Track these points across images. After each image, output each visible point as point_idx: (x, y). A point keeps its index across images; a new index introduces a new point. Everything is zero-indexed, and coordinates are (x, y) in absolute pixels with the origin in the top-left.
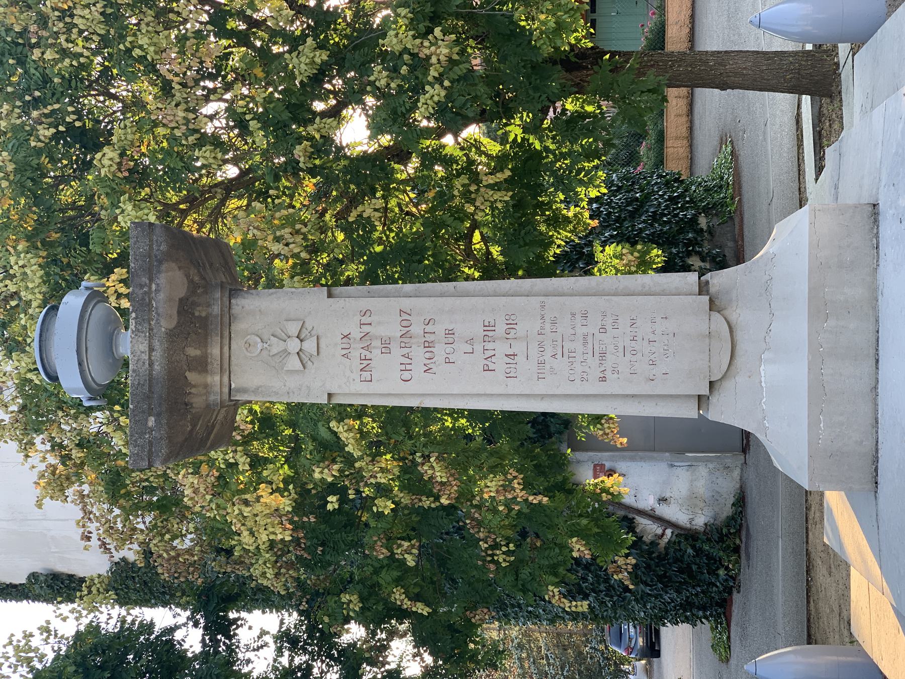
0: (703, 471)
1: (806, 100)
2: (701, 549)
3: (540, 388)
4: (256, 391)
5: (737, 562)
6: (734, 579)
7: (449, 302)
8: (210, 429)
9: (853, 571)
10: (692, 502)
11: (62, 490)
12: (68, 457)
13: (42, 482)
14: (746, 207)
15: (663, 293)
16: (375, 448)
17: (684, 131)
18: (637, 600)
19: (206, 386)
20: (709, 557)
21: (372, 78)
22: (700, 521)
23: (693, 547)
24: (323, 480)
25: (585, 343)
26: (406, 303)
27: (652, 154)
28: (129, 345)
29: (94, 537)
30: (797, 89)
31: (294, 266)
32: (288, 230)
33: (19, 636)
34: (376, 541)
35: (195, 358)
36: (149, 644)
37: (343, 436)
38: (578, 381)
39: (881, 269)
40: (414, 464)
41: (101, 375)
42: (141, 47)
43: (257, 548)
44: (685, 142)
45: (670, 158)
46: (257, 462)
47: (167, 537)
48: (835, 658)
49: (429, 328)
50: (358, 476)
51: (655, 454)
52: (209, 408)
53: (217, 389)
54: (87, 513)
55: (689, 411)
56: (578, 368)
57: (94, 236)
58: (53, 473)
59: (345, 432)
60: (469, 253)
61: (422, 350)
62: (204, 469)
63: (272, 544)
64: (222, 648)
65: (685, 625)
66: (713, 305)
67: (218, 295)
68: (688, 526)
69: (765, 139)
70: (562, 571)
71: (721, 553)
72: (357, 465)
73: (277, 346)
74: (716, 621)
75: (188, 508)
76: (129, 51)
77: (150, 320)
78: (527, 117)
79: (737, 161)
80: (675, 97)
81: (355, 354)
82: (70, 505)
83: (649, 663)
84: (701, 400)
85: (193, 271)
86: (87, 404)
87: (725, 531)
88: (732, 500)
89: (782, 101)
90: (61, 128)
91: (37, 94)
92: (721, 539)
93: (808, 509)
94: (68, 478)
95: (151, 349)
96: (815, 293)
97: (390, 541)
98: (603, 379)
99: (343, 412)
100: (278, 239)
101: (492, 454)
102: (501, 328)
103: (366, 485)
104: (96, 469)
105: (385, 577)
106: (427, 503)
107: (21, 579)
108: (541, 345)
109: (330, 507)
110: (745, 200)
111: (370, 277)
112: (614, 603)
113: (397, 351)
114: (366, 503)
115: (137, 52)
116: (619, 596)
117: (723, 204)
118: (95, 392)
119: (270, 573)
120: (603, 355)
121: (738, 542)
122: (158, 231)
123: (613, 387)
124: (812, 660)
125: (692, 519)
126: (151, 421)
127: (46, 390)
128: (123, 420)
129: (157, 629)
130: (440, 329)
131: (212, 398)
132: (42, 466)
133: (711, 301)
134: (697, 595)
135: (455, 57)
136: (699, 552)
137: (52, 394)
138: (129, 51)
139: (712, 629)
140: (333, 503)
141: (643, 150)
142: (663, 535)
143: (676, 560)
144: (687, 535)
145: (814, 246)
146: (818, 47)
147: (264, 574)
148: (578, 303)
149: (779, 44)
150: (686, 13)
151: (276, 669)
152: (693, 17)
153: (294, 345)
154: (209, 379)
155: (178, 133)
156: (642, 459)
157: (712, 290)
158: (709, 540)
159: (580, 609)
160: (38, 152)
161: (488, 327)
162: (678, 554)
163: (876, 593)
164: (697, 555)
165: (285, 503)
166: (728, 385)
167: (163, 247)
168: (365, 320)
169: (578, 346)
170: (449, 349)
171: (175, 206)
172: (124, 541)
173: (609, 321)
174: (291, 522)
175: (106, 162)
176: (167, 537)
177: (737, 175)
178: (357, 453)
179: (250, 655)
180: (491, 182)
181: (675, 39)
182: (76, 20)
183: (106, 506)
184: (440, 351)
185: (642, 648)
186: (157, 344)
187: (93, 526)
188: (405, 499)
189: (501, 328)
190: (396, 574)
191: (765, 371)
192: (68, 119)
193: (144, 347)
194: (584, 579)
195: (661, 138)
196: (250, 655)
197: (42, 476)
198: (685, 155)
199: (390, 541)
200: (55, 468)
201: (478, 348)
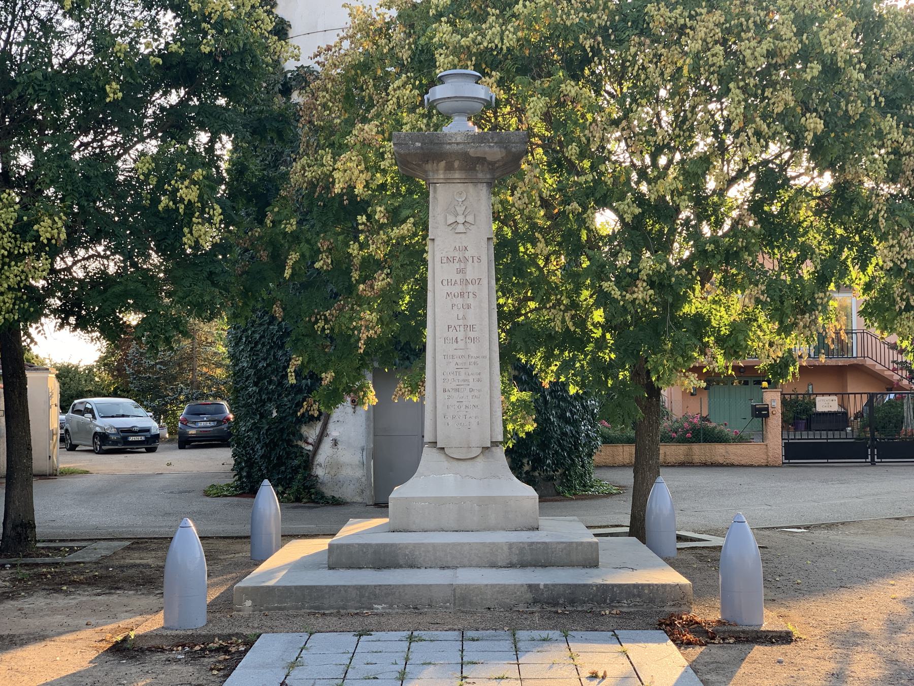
0: (359, 473)
2: (298, 472)
3: (439, 357)
4: (435, 198)
7: (486, 305)
10: (336, 465)
14: (567, 503)
15: (492, 423)
18: (254, 424)
19: (437, 170)
20: (292, 479)
21: (623, 250)
22: (319, 472)
23: (299, 466)
25: (464, 381)
26: (485, 282)
34: (329, 240)
38: (443, 377)
40: (382, 269)
44: (628, 461)
45: (614, 449)
51: (372, 436)
55: (428, 438)
56: (451, 377)
58: (371, 24)
61: (459, 291)
65: (233, 462)
67: (488, 176)
68: (316, 463)
69: (615, 513)
70: (312, 366)
71: (295, 488)
73: (460, 210)
74: (236, 487)
79: (604, 497)
81: (456, 254)
85: (501, 163)
87: (313, 491)
88: (337, 496)
92: (305, 488)
95: (458, 144)
96: (492, 499)
97: (329, 250)
98: (445, 391)
102: (472, 334)
103: (367, 237)
105: (305, 247)
106: (355, 275)
110: (572, 502)
112: (251, 405)
116: (257, 409)
117: (570, 488)
120: (457, 390)
121: (304, 500)
123: (440, 395)
124: (273, 520)
125: (321, 466)
126: (418, 144)
130: (471, 301)
131: (431, 174)
133: (488, 448)
134: (260, 470)
135: (637, 302)
136: (295, 470)
139: (228, 485)
142: (308, 443)
143: (288, 454)
144: (308, 461)
148: (486, 376)
152: (732, 465)
153: (461, 219)
154: (441, 172)
156: (368, 426)
157: (494, 449)
158: (305, 478)
159: (290, 378)
160: (576, 39)
161: (472, 328)
162: (293, 456)
164: (293, 470)
166: (442, 457)
167: (514, 150)
169: (463, 377)
173: (476, 393)
180: (567, 318)
184: (459, 301)
185: (186, 433)
186: (461, 146)
189: (472, 334)
193: (459, 140)
194: (270, 382)
198: (617, 461)
199: (329, 250)
201: (461, 322)
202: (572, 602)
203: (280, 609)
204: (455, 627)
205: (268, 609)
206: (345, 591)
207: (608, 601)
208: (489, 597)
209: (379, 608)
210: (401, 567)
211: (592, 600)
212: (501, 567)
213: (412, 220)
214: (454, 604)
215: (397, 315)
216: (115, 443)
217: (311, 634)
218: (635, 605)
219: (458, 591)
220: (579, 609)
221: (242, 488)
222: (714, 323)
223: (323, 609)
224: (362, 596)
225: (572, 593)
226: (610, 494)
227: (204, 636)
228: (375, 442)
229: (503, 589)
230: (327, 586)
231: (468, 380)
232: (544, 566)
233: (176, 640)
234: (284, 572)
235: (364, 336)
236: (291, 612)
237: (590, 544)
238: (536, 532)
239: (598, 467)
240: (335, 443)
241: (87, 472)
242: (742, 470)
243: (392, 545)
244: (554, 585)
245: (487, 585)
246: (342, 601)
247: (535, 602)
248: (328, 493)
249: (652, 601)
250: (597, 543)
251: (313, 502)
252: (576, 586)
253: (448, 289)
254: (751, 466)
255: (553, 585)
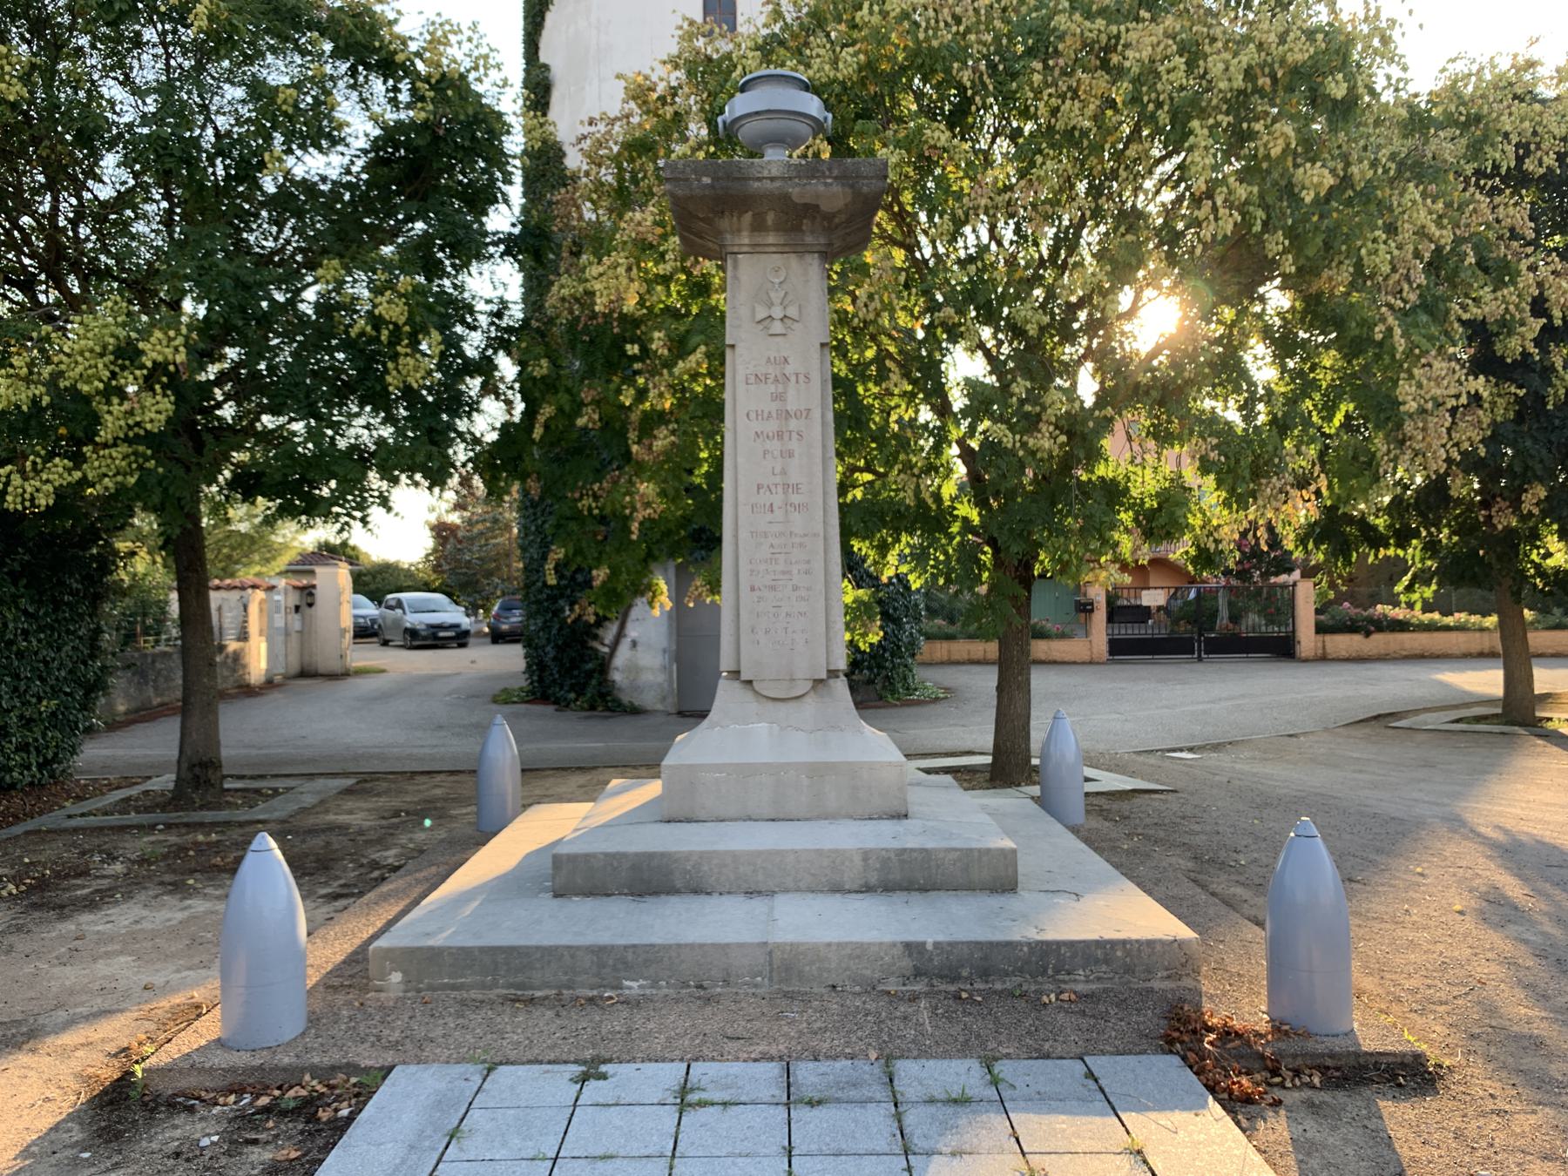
0: (661, 678)
1: (988, 759)
3: (743, 534)
4: (735, 277)
5: (582, 709)
6: (567, 706)
7: (818, 452)
8: (699, 235)
9: (591, 804)
10: (633, 669)
11: (634, 98)
12: (664, 103)
13: (640, 79)
16: (678, 389)
17: (956, 657)
19: (739, 231)
22: (617, 677)
24: (651, 340)
25: (784, 573)
26: (817, 414)
27: (935, 630)
28: (775, 158)
29: (593, 129)
30: (997, 751)
31: (846, 312)
32: (879, 306)
33: (499, 58)
35: (764, 220)
36: (493, 181)
37: (692, 358)
39: (851, 823)
40: (667, 423)
41: (746, 132)
42: (1043, 163)
43: (587, 280)
46: (665, 280)
47: (595, 196)
48: (510, 790)
49: (794, 435)
50: (654, 372)
52: (719, 233)
53: (737, 241)
54: (612, 122)
55: (726, 663)
57: (872, 125)
59: (697, 359)
60: (854, 469)
62: (659, 231)
63: (591, 294)
64: (492, 249)
66: (818, 682)
67: (822, 241)
70: (579, 559)
72: (665, 371)
73: (776, 296)
75: (621, 217)
76: (1040, 152)
77: (800, 177)
78: (976, 520)
80: (992, 649)
82: (619, 106)
83: (486, 635)
84: (735, 674)
85: (843, 217)
86: (720, 120)
89: (988, 741)
90: (970, 92)
91: (1001, 67)
93: (634, 767)
94: (645, 102)
95: (772, 179)
97: (597, 403)
98: (753, 589)
99: (717, 358)
100: (871, 297)
101: (677, 490)
102: (796, 499)
104: (653, 130)
105: (564, 398)
106: (632, 435)
107: (544, 57)
108: (782, 534)
109: (628, 347)
111: (837, 381)
113: (773, 407)
114: (630, 380)
115: (1039, 159)
117: (893, 692)
118: (731, 127)
119: (565, 292)
120: (773, 588)
122: (880, 184)
127: (726, 81)
128: (701, 155)
129: (505, 188)
130: (794, 445)
132: (654, 78)
133: (821, 681)
135: (1039, 455)
136: (590, 674)
137: (722, 87)
138: (1040, 152)
139: (521, 689)
140: (633, 349)
141: (939, 622)
144: (604, 665)
145: (872, 766)
146: (1035, 769)
147: (562, 286)
148: (818, 566)
149: (1037, 737)
150: (1057, 656)
151: (473, 297)
152: (1054, 662)
153: (777, 312)
154: (745, 233)
155: (965, 200)
156: (670, 626)
157: (832, 681)
158: (600, 684)
160: (948, 71)
161: (796, 488)
163: (574, 824)
165: (630, 304)
166: (749, 696)
167: (865, 189)
168: (801, 378)
170: (777, 453)
171: (896, 199)
172: (589, 157)
173: (803, 593)
174: (612, 311)
175: (937, 134)
176: (595, 196)
177: (918, 703)
178: (676, 371)
179: (487, 275)
181: (1040, 648)
182: (1068, 102)
183: (621, 139)
184: (775, 446)
186: (777, 184)
187: (602, 127)
188: (635, 417)
189: (796, 499)
190: (567, 408)
191: (762, 727)
192: (977, 98)
193: (775, 172)
195: (950, 637)
196: (487, 275)
197: (646, 78)
199: (597, 403)
200: (654, 90)
201: (778, 479)
202: (985, 974)
203: (454, 987)
204: (773, 1051)
205: (432, 988)
206: (572, 957)
207: (1050, 972)
208: (833, 965)
209: (633, 986)
210: (673, 891)
211: (1021, 970)
212: (849, 892)
213: (703, 348)
214: (771, 979)
215: (691, 490)
216: (425, 638)
217: (490, 1070)
218: (1099, 979)
219: (777, 954)
220: (998, 986)
221: (534, 693)
222: (1134, 493)
223: (533, 988)
224: (602, 965)
225: (985, 958)
226: (937, 699)
227: (285, 1069)
228: (678, 644)
229: (859, 951)
230: (537, 948)
231: (789, 572)
232: (924, 889)
233: (230, 1079)
234: (475, 904)
235: (639, 516)
236: (474, 994)
237: (1003, 852)
238: (905, 822)
239: (924, 664)
240: (634, 644)
241: (383, 671)
242: (1074, 668)
243: (663, 855)
244: (952, 944)
245: (829, 945)
246: (566, 973)
247: (918, 973)
248: (625, 699)
249: (1129, 970)
250: (1014, 852)
251: (609, 709)
252: (992, 945)
253: (757, 426)
254: (1075, 663)
255: (950, 944)
